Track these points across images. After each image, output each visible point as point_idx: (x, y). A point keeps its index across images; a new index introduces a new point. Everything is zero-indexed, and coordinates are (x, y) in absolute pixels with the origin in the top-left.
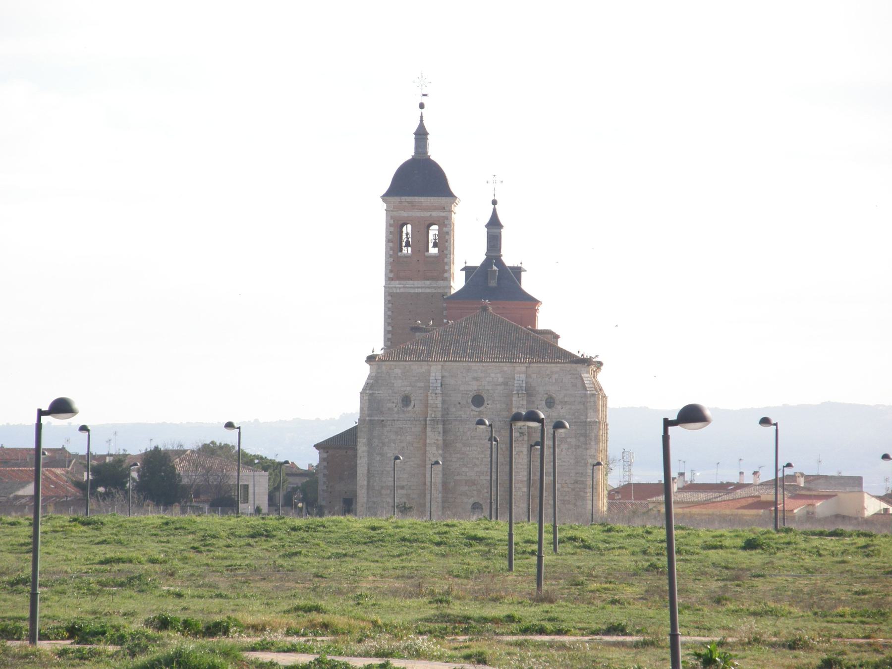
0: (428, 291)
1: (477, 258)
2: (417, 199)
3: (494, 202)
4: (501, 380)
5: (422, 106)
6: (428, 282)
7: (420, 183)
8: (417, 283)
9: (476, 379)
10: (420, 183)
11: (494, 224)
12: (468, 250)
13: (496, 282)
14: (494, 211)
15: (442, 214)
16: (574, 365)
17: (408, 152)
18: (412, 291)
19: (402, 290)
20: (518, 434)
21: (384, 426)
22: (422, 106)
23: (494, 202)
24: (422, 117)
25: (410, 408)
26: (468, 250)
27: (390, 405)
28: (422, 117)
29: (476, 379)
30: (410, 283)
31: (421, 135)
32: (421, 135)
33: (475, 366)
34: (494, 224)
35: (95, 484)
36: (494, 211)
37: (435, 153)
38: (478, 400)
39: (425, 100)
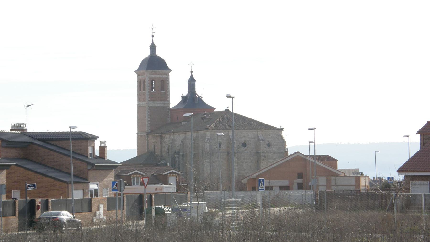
0: (162, 105)
1: (185, 92)
2: (158, 71)
3: (192, 72)
4: (253, 137)
5: (153, 36)
6: (162, 102)
7: (154, 70)
8: (158, 102)
9: (244, 136)
10: (154, 70)
11: (192, 82)
12: (176, 94)
13: (192, 100)
14: (192, 75)
15: (166, 76)
16: (278, 131)
17: (147, 53)
18: (156, 105)
19: (153, 105)
20: (263, 157)
21: (213, 155)
22: (153, 36)
23: (192, 72)
24: (153, 40)
25: (222, 148)
26: (176, 94)
27: (215, 147)
28: (153, 40)
29: (244, 136)
30: (156, 102)
31: (153, 47)
32: (153, 47)
33: (244, 132)
34: (192, 82)
35: (390, 195)
36: (192, 75)
37: (159, 53)
38: (244, 145)
39: (154, 34)
